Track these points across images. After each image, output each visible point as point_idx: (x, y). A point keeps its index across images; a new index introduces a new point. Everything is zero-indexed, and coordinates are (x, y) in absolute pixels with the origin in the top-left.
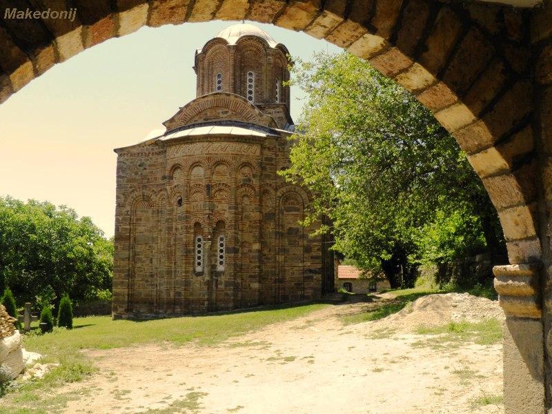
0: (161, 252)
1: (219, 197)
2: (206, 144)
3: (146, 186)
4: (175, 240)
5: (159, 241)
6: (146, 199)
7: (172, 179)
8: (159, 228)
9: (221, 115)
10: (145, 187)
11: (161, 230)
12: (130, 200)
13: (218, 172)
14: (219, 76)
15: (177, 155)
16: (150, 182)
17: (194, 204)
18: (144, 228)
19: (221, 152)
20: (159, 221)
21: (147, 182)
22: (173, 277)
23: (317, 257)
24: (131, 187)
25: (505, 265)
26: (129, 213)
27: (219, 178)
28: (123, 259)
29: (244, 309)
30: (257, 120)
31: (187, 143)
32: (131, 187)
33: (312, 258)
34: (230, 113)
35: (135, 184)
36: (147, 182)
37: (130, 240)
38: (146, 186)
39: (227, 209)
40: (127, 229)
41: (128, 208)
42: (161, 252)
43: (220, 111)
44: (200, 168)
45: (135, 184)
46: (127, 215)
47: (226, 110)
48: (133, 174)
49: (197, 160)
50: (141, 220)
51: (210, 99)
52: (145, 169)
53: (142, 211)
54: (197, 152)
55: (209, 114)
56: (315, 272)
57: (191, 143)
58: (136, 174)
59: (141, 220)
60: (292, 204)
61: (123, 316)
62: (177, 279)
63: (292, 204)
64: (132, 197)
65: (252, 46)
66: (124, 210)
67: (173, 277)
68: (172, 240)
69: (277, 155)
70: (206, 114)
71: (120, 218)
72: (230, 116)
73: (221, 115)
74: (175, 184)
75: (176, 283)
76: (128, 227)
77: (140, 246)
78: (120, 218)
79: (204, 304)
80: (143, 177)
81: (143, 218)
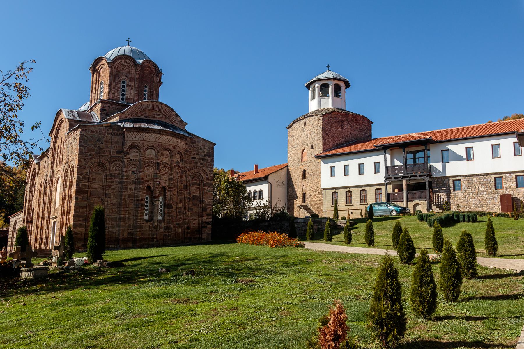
0: (114, 205)
1: (163, 171)
2: (158, 135)
3: (102, 156)
4: (129, 197)
5: (112, 196)
6: (101, 165)
7: (129, 154)
8: (113, 187)
9: (156, 116)
10: (101, 156)
11: (114, 189)
12: (89, 164)
13: (164, 155)
14: (124, 82)
15: (134, 139)
16: (105, 153)
17: (146, 173)
18: (97, 186)
19: (167, 142)
20: (113, 182)
21: (103, 153)
22: (127, 222)
23: (209, 215)
24: (90, 155)
25: (7, 238)
26: (88, 174)
27: (165, 159)
28: (82, 208)
29: (122, 246)
30: (179, 124)
31: (144, 132)
32: (90, 155)
33: (207, 215)
34: (161, 116)
35: (94, 153)
36: (103, 153)
37: (88, 193)
38: (102, 156)
39: (167, 179)
40: (85, 185)
41: (88, 170)
42: (114, 205)
43: (155, 113)
44: (153, 151)
45: (94, 153)
46: (87, 175)
47: (159, 113)
48: (93, 146)
49: (152, 145)
50: (95, 180)
51: (150, 103)
52: (102, 143)
53: (96, 174)
54: (151, 140)
55: (147, 114)
56: (208, 223)
57: (148, 133)
58: (95, 145)
59: (95, 180)
60: (196, 180)
61: (81, 250)
62: (130, 223)
63: (196, 180)
64: (91, 163)
65: (149, 67)
66: (85, 171)
67: (127, 222)
68: (127, 196)
69: (190, 149)
70: (146, 113)
71: (81, 177)
72: (161, 118)
73: (156, 116)
74: (131, 158)
75: (130, 226)
76: (87, 184)
77: (94, 199)
78: (81, 177)
79: (153, 241)
80: (100, 149)
81: (97, 179)
